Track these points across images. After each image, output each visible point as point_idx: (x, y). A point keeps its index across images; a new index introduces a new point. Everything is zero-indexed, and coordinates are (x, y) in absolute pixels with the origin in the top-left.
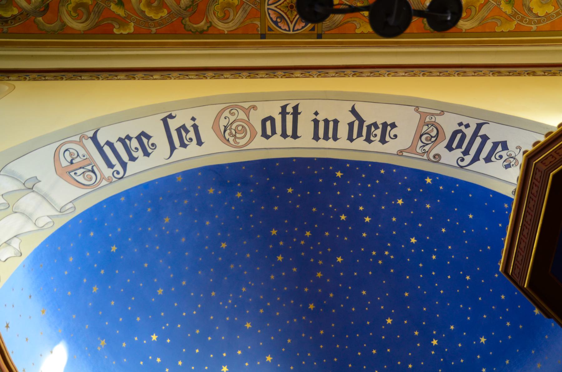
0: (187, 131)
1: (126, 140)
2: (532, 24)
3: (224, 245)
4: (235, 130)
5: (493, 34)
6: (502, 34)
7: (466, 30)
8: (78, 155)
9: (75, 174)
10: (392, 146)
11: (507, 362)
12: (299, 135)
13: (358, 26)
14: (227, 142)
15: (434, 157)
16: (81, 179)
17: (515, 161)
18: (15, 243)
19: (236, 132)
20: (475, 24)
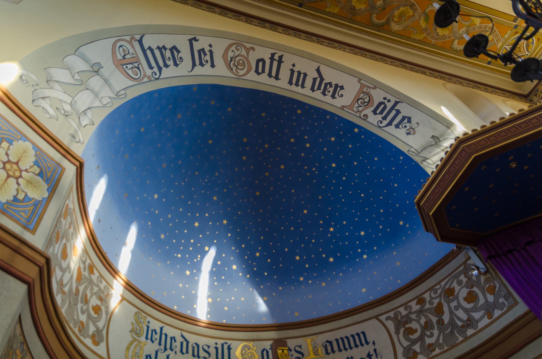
0: (205, 54)
1: (163, 50)
2: (433, 39)
3: (210, 142)
4: (238, 62)
5: (409, 38)
6: (414, 40)
7: (394, 31)
8: (129, 53)
9: (127, 67)
10: (338, 102)
11: (375, 248)
12: (280, 77)
13: (329, 6)
14: (231, 70)
15: (364, 116)
16: (130, 72)
17: (413, 131)
18: (89, 113)
19: (238, 64)
20: (401, 29)
